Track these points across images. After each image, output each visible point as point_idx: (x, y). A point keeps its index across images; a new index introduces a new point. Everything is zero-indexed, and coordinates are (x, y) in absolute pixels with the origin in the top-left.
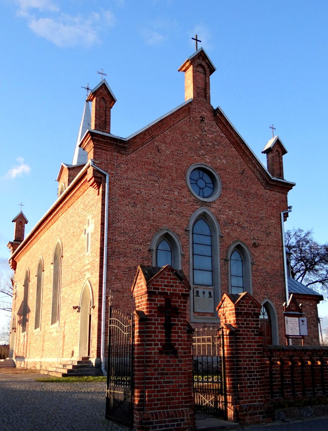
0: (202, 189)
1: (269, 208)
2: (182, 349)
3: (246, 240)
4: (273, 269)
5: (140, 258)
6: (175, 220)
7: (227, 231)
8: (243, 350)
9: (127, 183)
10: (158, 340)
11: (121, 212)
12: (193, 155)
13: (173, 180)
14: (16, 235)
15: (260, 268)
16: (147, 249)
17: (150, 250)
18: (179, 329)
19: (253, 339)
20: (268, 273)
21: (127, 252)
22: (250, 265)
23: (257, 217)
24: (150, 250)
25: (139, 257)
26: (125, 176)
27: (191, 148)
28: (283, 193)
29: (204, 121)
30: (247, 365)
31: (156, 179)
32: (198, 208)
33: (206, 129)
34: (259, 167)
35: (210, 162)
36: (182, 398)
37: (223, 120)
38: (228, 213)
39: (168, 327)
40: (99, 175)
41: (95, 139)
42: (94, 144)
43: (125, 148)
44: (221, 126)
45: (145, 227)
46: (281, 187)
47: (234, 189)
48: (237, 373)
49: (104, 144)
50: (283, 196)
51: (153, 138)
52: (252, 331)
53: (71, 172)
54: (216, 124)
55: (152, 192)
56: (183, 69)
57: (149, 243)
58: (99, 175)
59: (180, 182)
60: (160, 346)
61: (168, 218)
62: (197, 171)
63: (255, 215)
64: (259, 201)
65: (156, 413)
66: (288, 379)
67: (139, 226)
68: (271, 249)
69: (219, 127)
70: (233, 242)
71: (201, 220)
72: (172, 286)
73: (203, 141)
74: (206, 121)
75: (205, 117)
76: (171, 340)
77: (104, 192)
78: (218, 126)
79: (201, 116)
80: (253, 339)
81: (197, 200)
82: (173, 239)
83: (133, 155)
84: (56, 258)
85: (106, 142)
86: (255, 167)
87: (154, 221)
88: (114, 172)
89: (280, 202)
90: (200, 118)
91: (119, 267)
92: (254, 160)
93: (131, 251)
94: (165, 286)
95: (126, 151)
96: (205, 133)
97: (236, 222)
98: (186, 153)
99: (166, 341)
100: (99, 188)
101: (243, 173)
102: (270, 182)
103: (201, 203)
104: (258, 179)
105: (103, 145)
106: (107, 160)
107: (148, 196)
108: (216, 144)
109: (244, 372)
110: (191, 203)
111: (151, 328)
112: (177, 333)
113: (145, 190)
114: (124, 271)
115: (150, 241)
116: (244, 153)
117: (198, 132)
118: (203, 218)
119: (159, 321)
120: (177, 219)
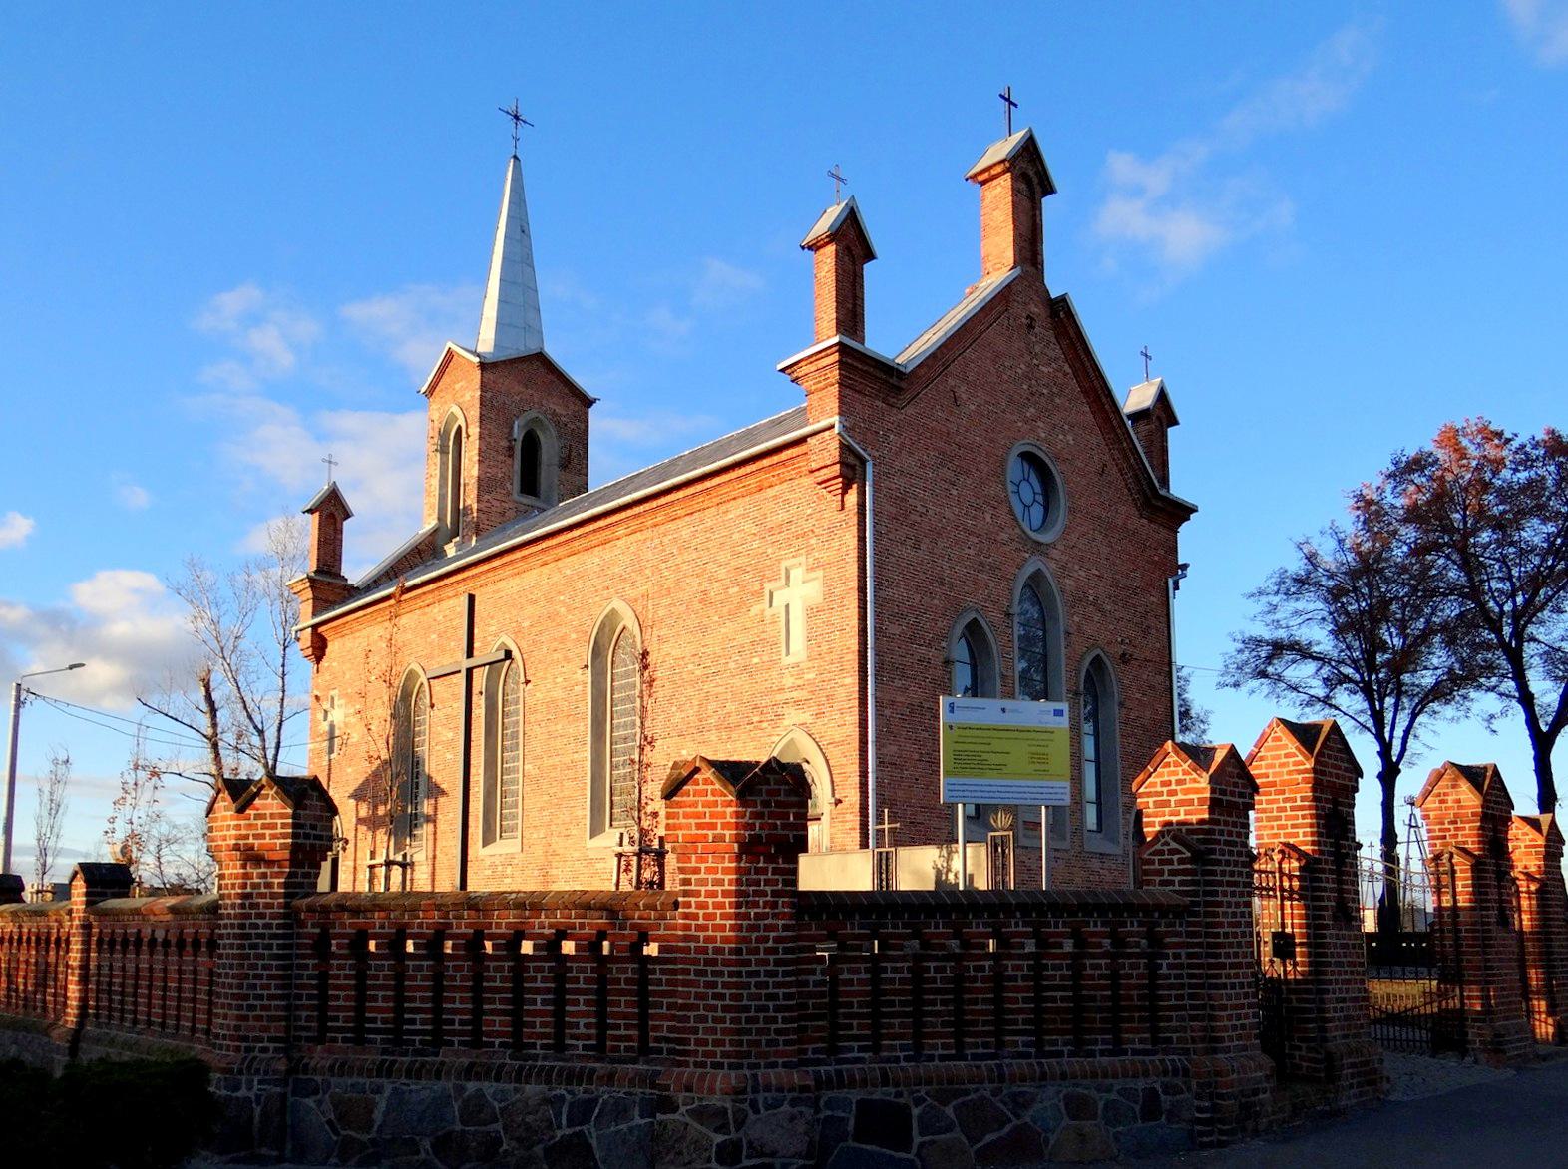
12: (1015, 418)
14: (319, 555)
16: (941, 659)
37: (1072, 332)
40: (851, 460)
42: (840, 374)
45: (936, 602)
48: (291, 975)
53: (489, 375)
56: (981, 178)
57: (943, 644)
58: (851, 460)
59: (994, 489)
66: (811, 989)
73: (1034, 382)
77: (861, 505)
83: (910, 410)
84: (598, 653)
104: (1129, 490)
110: (1016, 544)
116: (1107, 420)
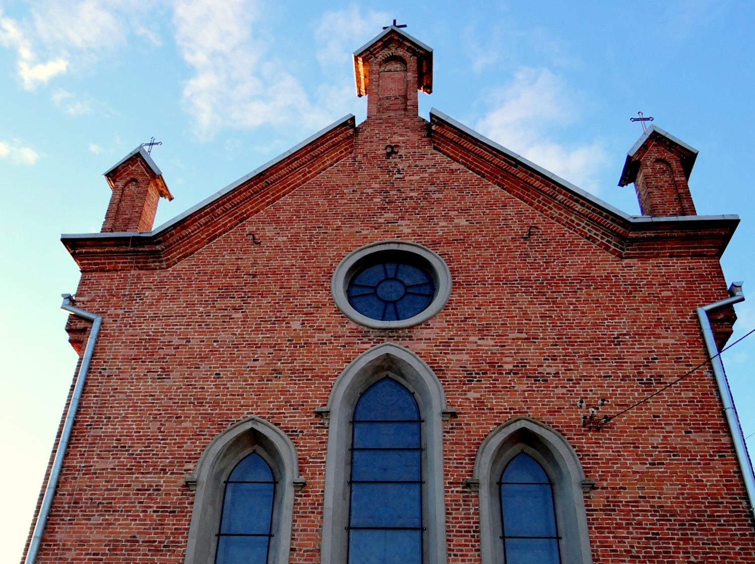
4: (694, 497)
5: (154, 512)
9: (153, 326)
11: (122, 396)
15: (625, 497)
16: (182, 482)
17: (189, 485)
20: (665, 514)
21: (114, 499)
22: (577, 494)
25: (150, 507)
34: (582, 205)
35: (414, 233)
38: (478, 346)
41: (81, 253)
43: (156, 255)
44: (449, 149)
46: (679, 238)
47: (498, 279)
49: (104, 259)
54: (435, 148)
55: (222, 336)
57: (191, 466)
67: (167, 424)
68: (668, 428)
69: (444, 153)
70: (499, 424)
75: (401, 144)
78: (440, 151)
81: (366, 329)
82: (271, 443)
83: (184, 265)
85: (108, 252)
86: (570, 210)
89: (687, 282)
90: (386, 149)
92: (560, 192)
93: (128, 494)
95: (161, 262)
98: (338, 228)
101: (529, 235)
102: (632, 235)
103: (378, 333)
105: (103, 261)
107: (207, 346)
110: (342, 341)
113: (200, 333)
114: (94, 554)
115: (194, 459)
116: (527, 186)
117: (377, 177)
118: (391, 375)
120: (292, 388)
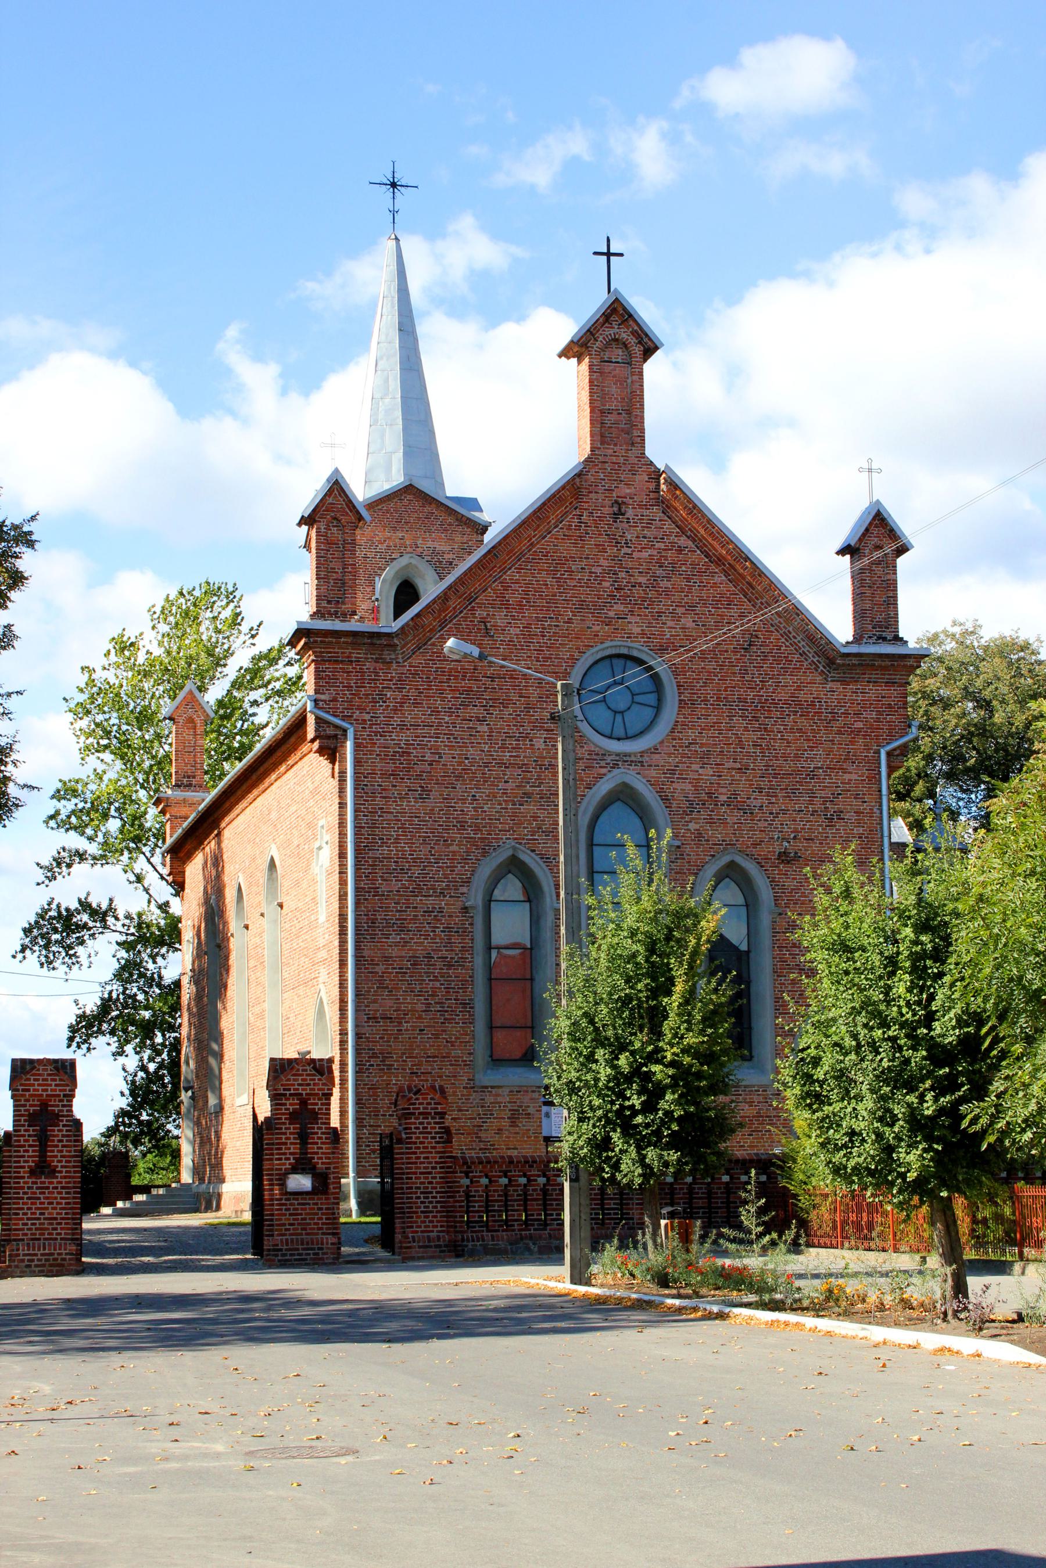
0: (622, 712)
1: (838, 738)
2: (323, 1163)
3: (755, 845)
6: (535, 818)
7: (692, 826)
8: (416, 1163)
10: (291, 1154)
11: (390, 817)
13: (528, 708)
18: (319, 1138)
19: (432, 1148)
21: (405, 919)
23: (797, 772)
24: (465, 909)
26: (397, 720)
27: (582, 605)
28: (890, 683)
29: (623, 514)
30: (421, 1183)
31: (481, 712)
32: (604, 775)
33: (629, 538)
36: (323, 1224)
39: (304, 1137)
50: (894, 692)
51: (471, 599)
52: (432, 1138)
57: (464, 890)
58: (330, 731)
60: (292, 1161)
61: (513, 816)
62: (604, 668)
63: (788, 766)
64: (803, 722)
65: (287, 1240)
70: (713, 856)
71: (618, 804)
72: (309, 1085)
74: (630, 513)
76: (307, 1153)
79: (616, 502)
80: (432, 1148)
87: (477, 829)
88: (367, 717)
91: (386, 958)
94: (299, 1085)
96: (629, 551)
97: (723, 798)
99: (301, 1153)
100: (334, 764)
106: (349, 687)
108: (664, 574)
109: (416, 1193)
111: (281, 1138)
112: (317, 1143)
113: (451, 747)
119: (289, 1132)
